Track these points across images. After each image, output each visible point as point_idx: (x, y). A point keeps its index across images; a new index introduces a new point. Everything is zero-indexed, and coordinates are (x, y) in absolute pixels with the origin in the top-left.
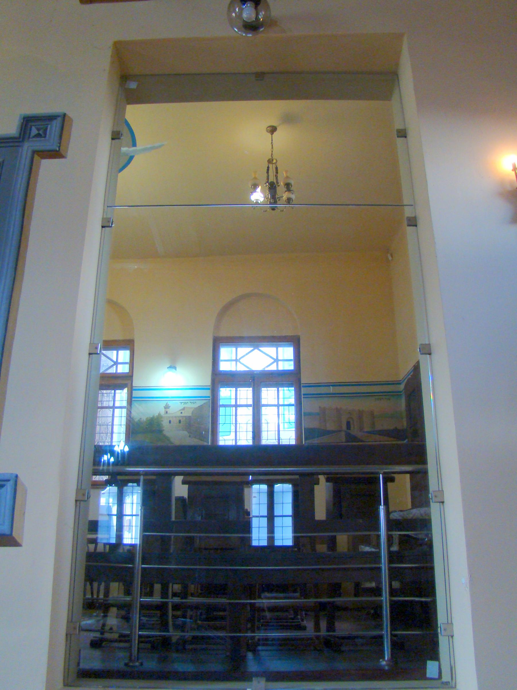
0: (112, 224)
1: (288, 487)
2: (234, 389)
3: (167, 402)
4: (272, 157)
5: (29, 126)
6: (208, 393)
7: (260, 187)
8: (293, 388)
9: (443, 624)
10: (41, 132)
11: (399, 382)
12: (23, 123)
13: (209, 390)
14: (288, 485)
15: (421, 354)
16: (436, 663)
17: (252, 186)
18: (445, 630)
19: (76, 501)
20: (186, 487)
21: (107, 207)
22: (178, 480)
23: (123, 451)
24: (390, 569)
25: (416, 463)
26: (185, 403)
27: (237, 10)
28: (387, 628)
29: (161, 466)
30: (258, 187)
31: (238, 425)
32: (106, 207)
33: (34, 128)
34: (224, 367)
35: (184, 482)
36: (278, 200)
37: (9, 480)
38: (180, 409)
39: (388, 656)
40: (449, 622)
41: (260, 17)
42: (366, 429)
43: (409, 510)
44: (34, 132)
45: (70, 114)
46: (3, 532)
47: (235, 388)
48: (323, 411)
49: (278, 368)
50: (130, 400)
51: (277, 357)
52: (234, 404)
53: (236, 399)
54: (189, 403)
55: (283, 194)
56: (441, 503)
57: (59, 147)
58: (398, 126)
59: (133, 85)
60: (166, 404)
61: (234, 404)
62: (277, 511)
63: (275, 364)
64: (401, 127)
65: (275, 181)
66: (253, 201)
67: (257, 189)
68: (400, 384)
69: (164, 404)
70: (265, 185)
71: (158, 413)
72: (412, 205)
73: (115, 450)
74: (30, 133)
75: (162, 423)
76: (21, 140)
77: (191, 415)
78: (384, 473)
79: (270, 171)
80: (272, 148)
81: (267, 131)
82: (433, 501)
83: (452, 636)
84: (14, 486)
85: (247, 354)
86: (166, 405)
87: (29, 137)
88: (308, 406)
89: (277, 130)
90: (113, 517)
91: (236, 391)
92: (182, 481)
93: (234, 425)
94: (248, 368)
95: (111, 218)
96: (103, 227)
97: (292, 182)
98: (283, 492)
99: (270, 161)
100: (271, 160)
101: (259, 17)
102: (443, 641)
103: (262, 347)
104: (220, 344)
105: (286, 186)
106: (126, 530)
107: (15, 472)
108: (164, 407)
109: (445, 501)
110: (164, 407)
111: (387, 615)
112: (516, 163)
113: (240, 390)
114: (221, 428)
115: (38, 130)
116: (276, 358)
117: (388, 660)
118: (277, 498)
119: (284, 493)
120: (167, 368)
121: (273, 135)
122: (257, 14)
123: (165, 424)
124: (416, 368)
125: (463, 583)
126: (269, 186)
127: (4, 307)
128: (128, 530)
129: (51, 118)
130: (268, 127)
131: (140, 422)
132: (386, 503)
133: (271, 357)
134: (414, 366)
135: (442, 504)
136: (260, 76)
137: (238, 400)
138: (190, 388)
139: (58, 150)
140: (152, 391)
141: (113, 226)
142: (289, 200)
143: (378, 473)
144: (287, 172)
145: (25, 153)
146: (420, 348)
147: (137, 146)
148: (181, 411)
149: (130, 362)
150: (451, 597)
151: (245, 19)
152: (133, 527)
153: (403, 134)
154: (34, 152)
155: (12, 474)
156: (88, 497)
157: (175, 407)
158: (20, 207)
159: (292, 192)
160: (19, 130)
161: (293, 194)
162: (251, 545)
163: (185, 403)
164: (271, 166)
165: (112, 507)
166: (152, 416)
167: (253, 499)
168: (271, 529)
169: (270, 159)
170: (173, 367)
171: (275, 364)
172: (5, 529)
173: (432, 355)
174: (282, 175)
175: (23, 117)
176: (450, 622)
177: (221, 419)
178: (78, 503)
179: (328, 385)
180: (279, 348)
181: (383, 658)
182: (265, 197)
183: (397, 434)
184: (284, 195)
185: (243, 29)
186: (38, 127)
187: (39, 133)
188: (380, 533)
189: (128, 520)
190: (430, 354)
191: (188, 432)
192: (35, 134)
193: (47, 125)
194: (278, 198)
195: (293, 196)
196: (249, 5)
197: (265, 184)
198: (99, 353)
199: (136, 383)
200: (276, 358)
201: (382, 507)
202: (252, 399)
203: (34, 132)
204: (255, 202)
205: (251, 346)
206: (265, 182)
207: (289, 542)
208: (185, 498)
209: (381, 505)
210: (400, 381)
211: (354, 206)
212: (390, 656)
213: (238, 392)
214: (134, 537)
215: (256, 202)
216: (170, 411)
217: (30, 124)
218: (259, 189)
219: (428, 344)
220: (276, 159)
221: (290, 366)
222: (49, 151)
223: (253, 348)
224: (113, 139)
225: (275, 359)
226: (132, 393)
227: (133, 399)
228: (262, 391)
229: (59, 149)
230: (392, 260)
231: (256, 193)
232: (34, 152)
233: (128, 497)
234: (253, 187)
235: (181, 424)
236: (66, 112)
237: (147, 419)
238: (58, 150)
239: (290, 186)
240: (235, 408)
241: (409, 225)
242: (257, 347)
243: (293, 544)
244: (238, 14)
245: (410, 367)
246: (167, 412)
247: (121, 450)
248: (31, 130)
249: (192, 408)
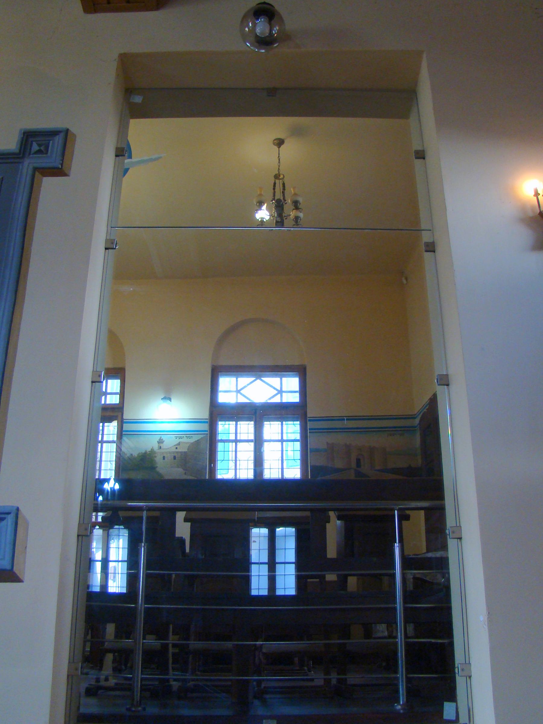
0: (116, 246)
1: (291, 530)
2: (234, 423)
3: (161, 436)
4: (279, 172)
6: (205, 427)
7: (266, 205)
8: (298, 422)
9: (460, 664)
10: (42, 148)
11: (413, 416)
12: (23, 138)
13: (207, 424)
14: (291, 528)
15: (438, 385)
16: (454, 704)
17: (258, 203)
18: (463, 670)
19: (78, 536)
20: (189, 524)
21: (110, 228)
22: (180, 516)
23: (113, 489)
24: (405, 609)
25: (432, 499)
26: (181, 438)
27: (251, 25)
28: (402, 672)
30: (264, 205)
31: (238, 462)
32: (109, 228)
33: (35, 145)
34: (223, 398)
35: (186, 520)
36: (284, 219)
37: (9, 513)
38: (175, 444)
39: (403, 699)
40: (466, 662)
41: (274, 32)
42: (377, 468)
43: (423, 554)
44: (35, 147)
45: (73, 130)
46: (4, 568)
47: (235, 422)
48: (331, 447)
49: (282, 401)
50: (121, 434)
51: (281, 388)
52: (234, 439)
53: (236, 433)
54: (185, 437)
55: (291, 213)
56: (459, 540)
57: (62, 165)
58: (416, 146)
59: (138, 99)
60: (160, 438)
61: (234, 439)
62: (279, 558)
63: (279, 395)
64: (420, 148)
65: (282, 198)
66: (258, 219)
67: (262, 206)
68: (415, 418)
69: (157, 438)
70: (271, 203)
71: (151, 448)
72: (430, 230)
73: (105, 488)
74: (31, 149)
75: (155, 459)
76: (21, 156)
77: (186, 450)
78: (399, 510)
79: (277, 185)
80: (279, 162)
81: (274, 144)
82: (451, 537)
83: (470, 677)
84: (14, 520)
85: (248, 385)
86: (159, 440)
87: (30, 154)
88: (314, 441)
89: (284, 143)
90: (96, 564)
91: (236, 425)
92: (184, 518)
93: (234, 461)
94: (249, 399)
95: (115, 240)
96: (106, 249)
97: (300, 199)
98: (285, 536)
99: (277, 177)
100: (278, 175)
101: (273, 32)
102: (460, 681)
103: (268, 377)
104: (219, 373)
105: (294, 204)
106: (110, 579)
107: (16, 505)
108: (158, 441)
109: (463, 536)
110: (158, 441)
111: (402, 657)
112: (537, 189)
113: (240, 424)
114: (220, 465)
115: (39, 145)
116: (279, 389)
117: (403, 704)
118: (279, 544)
119: (286, 537)
120: (161, 399)
121: (280, 149)
122: (271, 30)
123: (158, 459)
124: (433, 401)
125: (481, 620)
126: (276, 204)
127: (4, 332)
128: (113, 579)
129: (54, 133)
130: (274, 140)
131: (131, 458)
132: (401, 541)
133: (274, 388)
134: (430, 399)
135: (460, 541)
136: (272, 92)
137: (238, 435)
138: (187, 421)
139: (60, 167)
140: (140, 424)
141: (116, 248)
142: (297, 218)
143: (393, 510)
144: (294, 188)
145: (25, 171)
146: (437, 379)
147: (132, 158)
148: (176, 446)
149: (120, 392)
150: (465, 581)
151: (258, 34)
152: (119, 574)
153: (421, 155)
154: (35, 169)
155: (13, 507)
156: (91, 532)
157: (170, 442)
159: (300, 210)
160: (19, 146)
161: (301, 212)
162: (250, 594)
163: (181, 438)
164: (277, 181)
165: (95, 553)
166: (144, 452)
167: (252, 543)
168: (272, 580)
169: (277, 174)
170: (167, 398)
171: (279, 395)
172: (5, 564)
173: (450, 386)
174: (290, 191)
175: (23, 132)
176: (467, 662)
177: (220, 456)
178: (80, 538)
179: (341, 419)
180: (283, 379)
181: (398, 702)
182: (271, 215)
183: (410, 471)
184: (292, 213)
185: (257, 44)
187: (40, 149)
188: (395, 572)
189: (112, 567)
190: (448, 385)
191: (184, 469)
193: (50, 140)
194: (285, 216)
195: (301, 215)
196: (263, 20)
197: (272, 201)
198: (102, 381)
199: (127, 415)
200: (279, 389)
201: (397, 545)
202: (253, 434)
203: (35, 147)
204: (260, 220)
205: (253, 376)
206: (272, 199)
207: (292, 591)
208: (183, 539)
209: (396, 543)
210: (415, 415)
211: (369, 230)
212: (405, 700)
213: (238, 426)
214: (119, 586)
215: (261, 220)
216: (164, 446)
217: (30, 140)
218: (264, 207)
219: (446, 375)
220: (283, 175)
221: (295, 398)
222: (49, 168)
223: (255, 378)
224: (117, 156)
225: (278, 390)
226: (122, 427)
227: (124, 433)
228: (265, 425)
229: (62, 166)
230: (406, 284)
231: (261, 211)
232: (35, 169)
233: (112, 541)
234: (258, 204)
235: (175, 461)
236: (68, 127)
237: (138, 455)
238: (60, 167)
239: (299, 204)
240: (235, 443)
241: (426, 251)
242: (259, 377)
243: (296, 593)
244: (251, 29)
245: (426, 399)
246: (160, 448)
247: (111, 488)
248: (31, 146)
249: (188, 443)
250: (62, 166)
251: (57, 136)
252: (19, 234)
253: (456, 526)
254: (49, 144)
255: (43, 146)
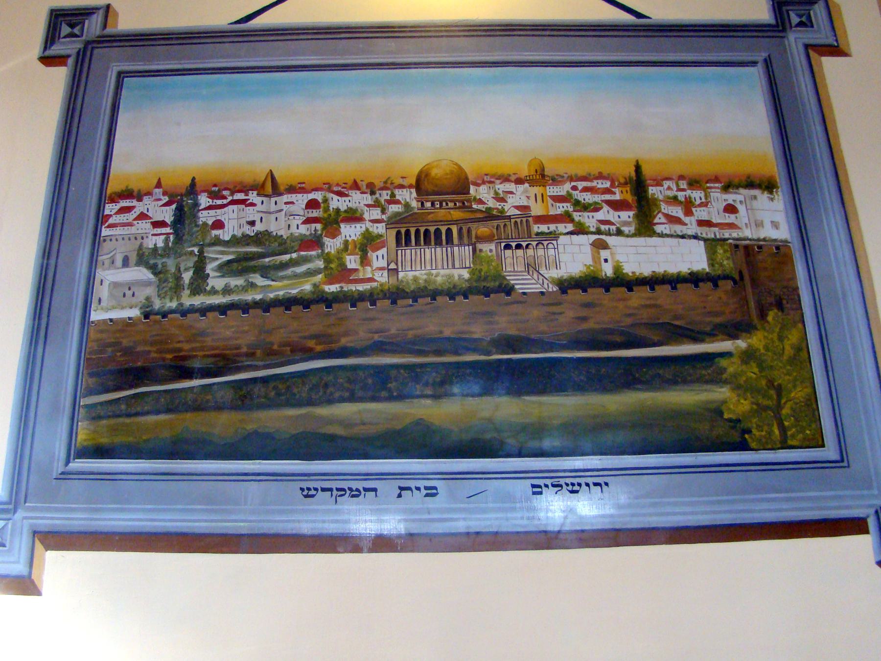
5: (785, 13)
10: (804, 19)
29: (409, 365)
57: (837, 41)
87: (59, 39)
115: (800, 16)
139: (836, 45)
158: (817, 119)
186: (798, 12)
192: (797, 22)
193: (810, 10)
203: (795, 20)
217: (784, 8)
229: (838, 44)
250: (838, 44)
251: (95, 16)
252: (819, 129)
253: (566, 246)
254: (809, 13)
255: (804, 17)
